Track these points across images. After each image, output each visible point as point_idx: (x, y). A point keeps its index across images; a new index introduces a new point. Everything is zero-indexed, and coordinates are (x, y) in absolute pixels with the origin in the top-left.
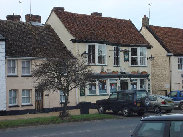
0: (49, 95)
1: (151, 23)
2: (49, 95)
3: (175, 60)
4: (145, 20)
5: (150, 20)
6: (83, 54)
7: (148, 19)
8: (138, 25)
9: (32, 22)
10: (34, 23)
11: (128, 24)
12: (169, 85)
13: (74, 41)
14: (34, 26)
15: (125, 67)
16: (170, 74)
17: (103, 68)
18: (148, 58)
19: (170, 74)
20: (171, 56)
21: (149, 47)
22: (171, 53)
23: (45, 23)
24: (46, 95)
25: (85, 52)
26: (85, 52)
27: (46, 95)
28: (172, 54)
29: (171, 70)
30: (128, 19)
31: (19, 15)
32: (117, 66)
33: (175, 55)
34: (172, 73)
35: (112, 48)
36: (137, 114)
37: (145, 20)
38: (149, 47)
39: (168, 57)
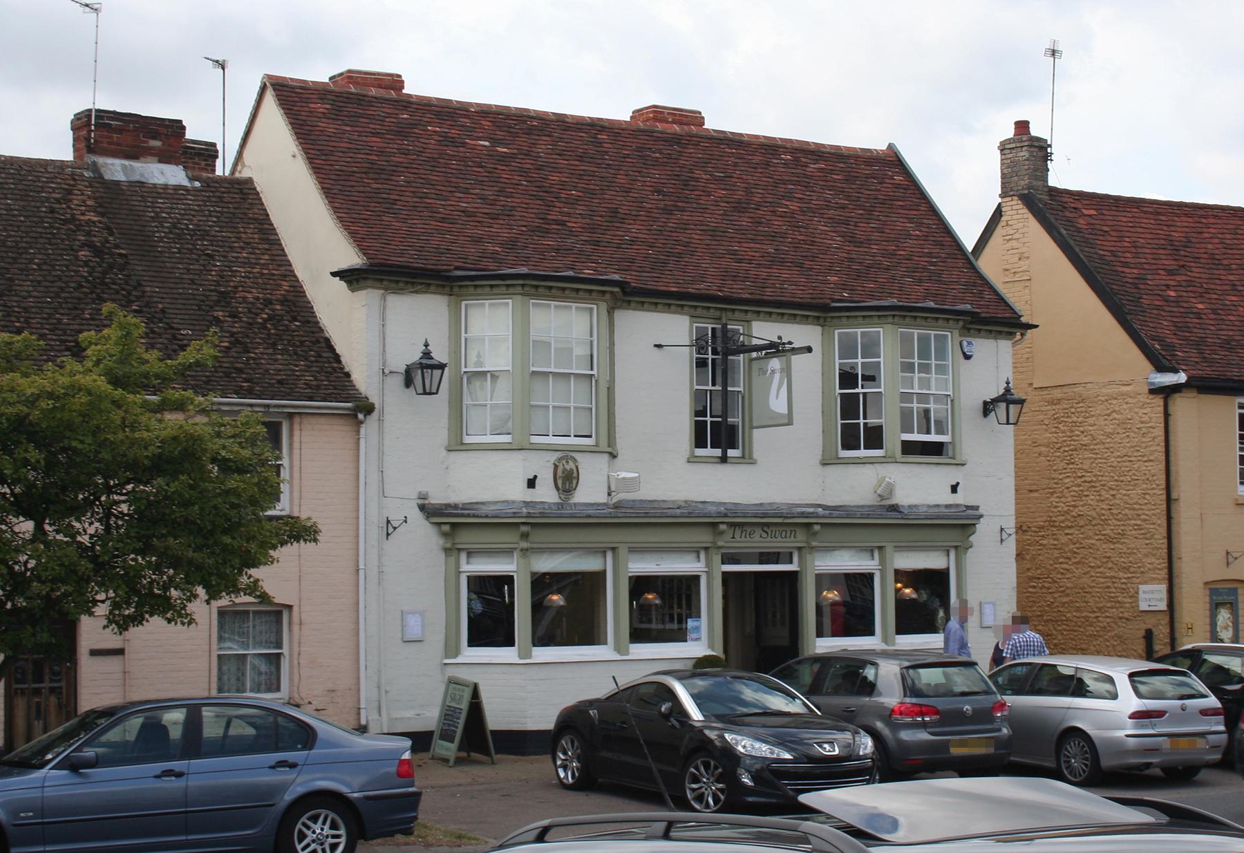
0: (120, 652)
1: (1061, 176)
2: (120, 652)
3: (1208, 428)
4: (1026, 154)
5: (1056, 150)
6: (995, 401)
7: (1041, 151)
8: (965, 192)
9: (110, 161)
10: (116, 169)
11: (882, 182)
12: (1164, 595)
13: (351, 277)
14: (117, 183)
15: (788, 466)
16: (1169, 518)
17: (571, 465)
18: (985, 403)
19: (1169, 518)
20: (1176, 389)
21: (1001, 320)
22: (1176, 371)
23: (233, 171)
24: (94, 653)
25: (427, 355)
26: (427, 355)
27: (94, 653)
28: (1182, 378)
29: (1174, 496)
30: (878, 144)
31: (206, 143)
32: (718, 452)
33: (1202, 386)
34: (1186, 515)
35: (676, 328)
36: (1219, 705)
37: (1026, 154)
38: (1001, 320)
39: (1158, 401)
